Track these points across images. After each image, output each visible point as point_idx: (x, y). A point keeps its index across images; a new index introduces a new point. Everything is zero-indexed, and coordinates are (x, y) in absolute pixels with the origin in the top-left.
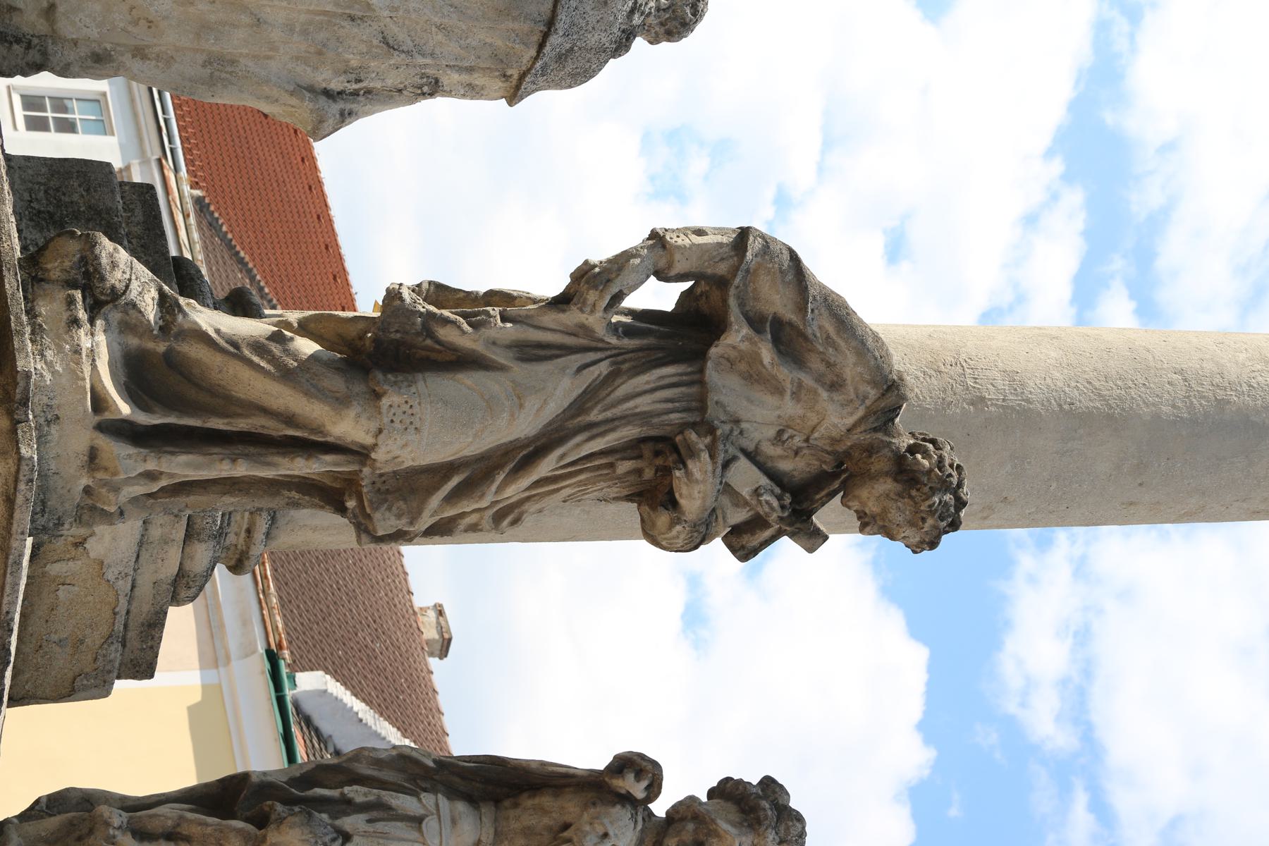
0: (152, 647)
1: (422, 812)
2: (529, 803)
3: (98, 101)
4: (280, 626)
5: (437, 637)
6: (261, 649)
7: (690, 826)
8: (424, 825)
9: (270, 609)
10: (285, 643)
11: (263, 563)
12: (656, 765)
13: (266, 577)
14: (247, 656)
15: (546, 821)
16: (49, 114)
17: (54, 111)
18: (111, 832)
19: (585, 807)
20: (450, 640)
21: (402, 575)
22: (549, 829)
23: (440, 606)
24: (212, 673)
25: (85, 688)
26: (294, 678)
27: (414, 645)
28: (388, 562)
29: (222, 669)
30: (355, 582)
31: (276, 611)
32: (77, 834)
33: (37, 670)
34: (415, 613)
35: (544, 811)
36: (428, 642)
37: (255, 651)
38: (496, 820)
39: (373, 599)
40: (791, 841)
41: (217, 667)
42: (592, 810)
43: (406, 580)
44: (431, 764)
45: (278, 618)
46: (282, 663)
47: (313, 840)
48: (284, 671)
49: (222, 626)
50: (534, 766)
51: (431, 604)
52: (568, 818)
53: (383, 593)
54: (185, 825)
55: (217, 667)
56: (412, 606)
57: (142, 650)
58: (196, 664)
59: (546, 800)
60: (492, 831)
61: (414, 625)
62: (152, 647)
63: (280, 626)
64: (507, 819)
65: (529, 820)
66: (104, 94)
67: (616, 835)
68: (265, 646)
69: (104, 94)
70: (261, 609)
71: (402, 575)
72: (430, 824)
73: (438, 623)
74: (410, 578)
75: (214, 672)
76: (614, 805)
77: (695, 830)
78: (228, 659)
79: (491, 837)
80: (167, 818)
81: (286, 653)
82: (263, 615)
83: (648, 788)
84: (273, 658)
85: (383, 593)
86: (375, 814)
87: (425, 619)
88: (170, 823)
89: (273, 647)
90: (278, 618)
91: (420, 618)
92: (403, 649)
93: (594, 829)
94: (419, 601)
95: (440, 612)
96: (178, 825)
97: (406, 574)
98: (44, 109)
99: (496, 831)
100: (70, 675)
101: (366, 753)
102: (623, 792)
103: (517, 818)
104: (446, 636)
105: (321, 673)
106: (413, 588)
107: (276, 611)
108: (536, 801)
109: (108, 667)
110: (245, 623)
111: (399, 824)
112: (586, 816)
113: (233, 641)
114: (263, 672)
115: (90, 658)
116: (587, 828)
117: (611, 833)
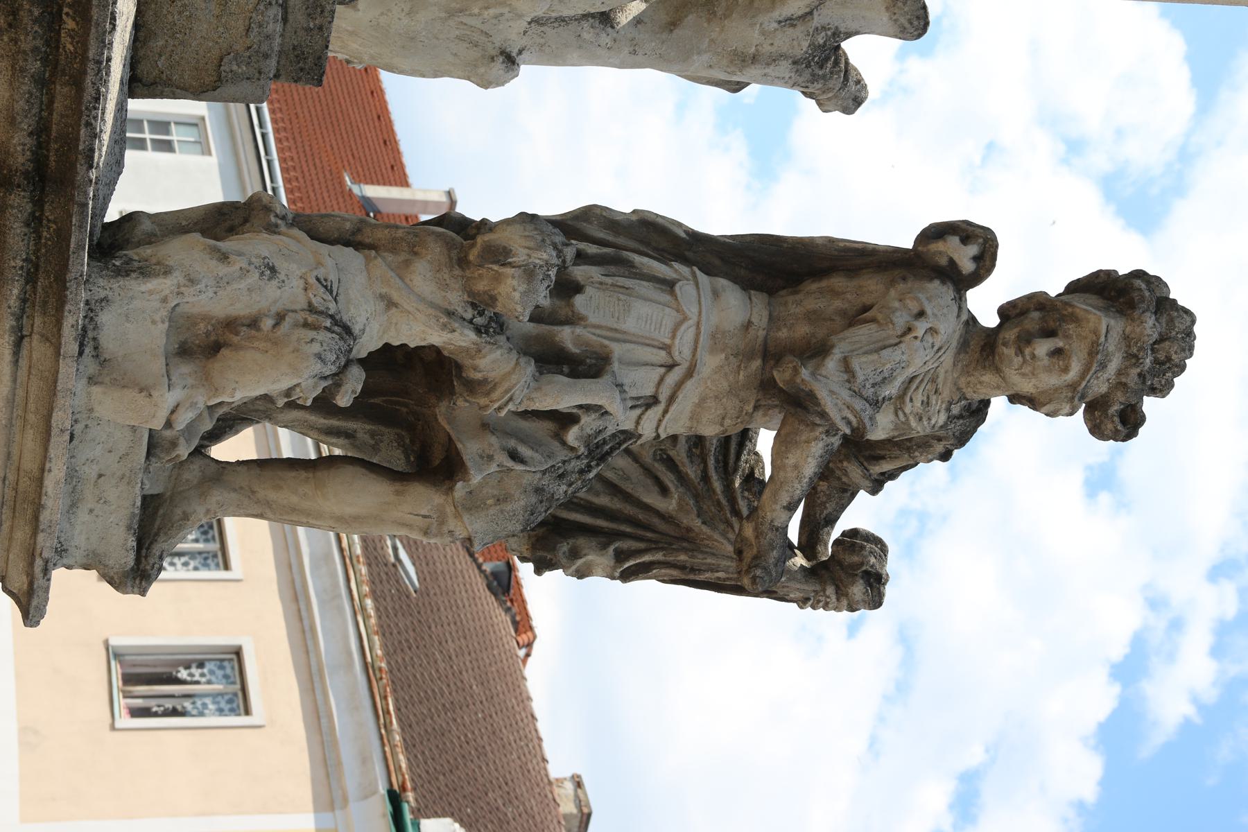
0: (320, 28)
1: (675, 276)
2: (814, 286)
3: (196, 123)
4: (404, 765)
5: (575, 811)
6: (382, 789)
7: (1036, 315)
8: (677, 288)
9: (393, 747)
10: (409, 785)
11: (386, 698)
12: (987, 231)
13: (388, 712)
14: (366, 797)
15: (838, 303)
16: (147, 136)
17: (151, 132)
18: (273, 219)
19: (892, 283)
20: (589, 815)
21: (536, 741)
22: (843, 313)
23: (579, 776)
24: (328, 816)
25: (236, 78)
26: (418, 825)
27: (549, 818)
28: (520, 724)
29: (338, 812)
30: (485, 738)
31: (399, 750)
32: (227, 224)
33: (173, 37)
34: (550, 783)
35: (835, 293)
36: (565, 816)
37: (375, 792)
38: (769, 304)
39: (504, 760)
40: (1175, 339)
41: (332, 809)
42: (901, 286)
43: (540, 746)
44: (683, 235)
45: (401, 757)
46: (406, 808)
47: (539, 238)
48: (408, 817)
49: (339, 764)
50: (820, 242)
51: (569, 775)
52: (867, 300)
53: (515, 756)
54: (367, 231)
55: (332, 809)
56: (547, 775)
57: (308, 30)
58: (310, 806)
59: (837, 282)
60: (765, 313)
61: (550, 796)
62: (320, 28)
63: (404, 765)
64: (786, 304)
65: (812, 303)
66: (203, 119)
67: (935, 315)
68: (387, 786)
69: (203, 119)
70: (383, 745)
71: (536, 741)
72: (685, 290)
73: (577, 796)
74: (545, 745)
75: (329, 815)
76: (931, 280)
77: (1043, 319)
78: (345, 800)
79: (765, 319)
80: (344, 219)
81: (410, 796)
82: (384, 752)
83: (977, 259)
84: (395, 799)
85: (515, 756)
86: (613, 269)
87: (562, 791)
88: (348, 226)
89: (396, 787)
90: (401, 757)
91: (556, 791)
92: (538, 819)
93: (905, 306)
94: (558, 768)
95: (578, 784)
96: (359, 230)
97: (540, 739)
98: (142, 131)
99: (770, 315)
100: (215, 53)
101: (598, 212)
102: (943, 261)
103: (799, 303)
104: (586, 810)
105: (448, 820)
106: (548, 756)
107: (399, 750)
108: (824, 283)
109: (265, 48)
110: (365, 760)
111: (645, 283)
112: (893, 293)
113: (351, 779)
114: (384, 815)
115: (241, 25)
116: (897, 304)
117: (929, 311)
